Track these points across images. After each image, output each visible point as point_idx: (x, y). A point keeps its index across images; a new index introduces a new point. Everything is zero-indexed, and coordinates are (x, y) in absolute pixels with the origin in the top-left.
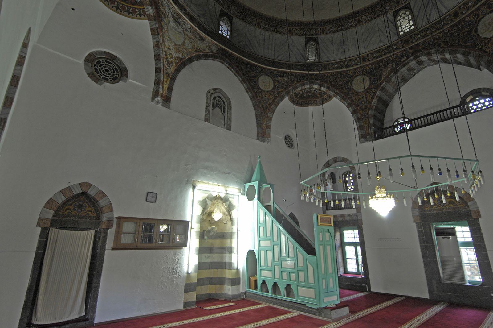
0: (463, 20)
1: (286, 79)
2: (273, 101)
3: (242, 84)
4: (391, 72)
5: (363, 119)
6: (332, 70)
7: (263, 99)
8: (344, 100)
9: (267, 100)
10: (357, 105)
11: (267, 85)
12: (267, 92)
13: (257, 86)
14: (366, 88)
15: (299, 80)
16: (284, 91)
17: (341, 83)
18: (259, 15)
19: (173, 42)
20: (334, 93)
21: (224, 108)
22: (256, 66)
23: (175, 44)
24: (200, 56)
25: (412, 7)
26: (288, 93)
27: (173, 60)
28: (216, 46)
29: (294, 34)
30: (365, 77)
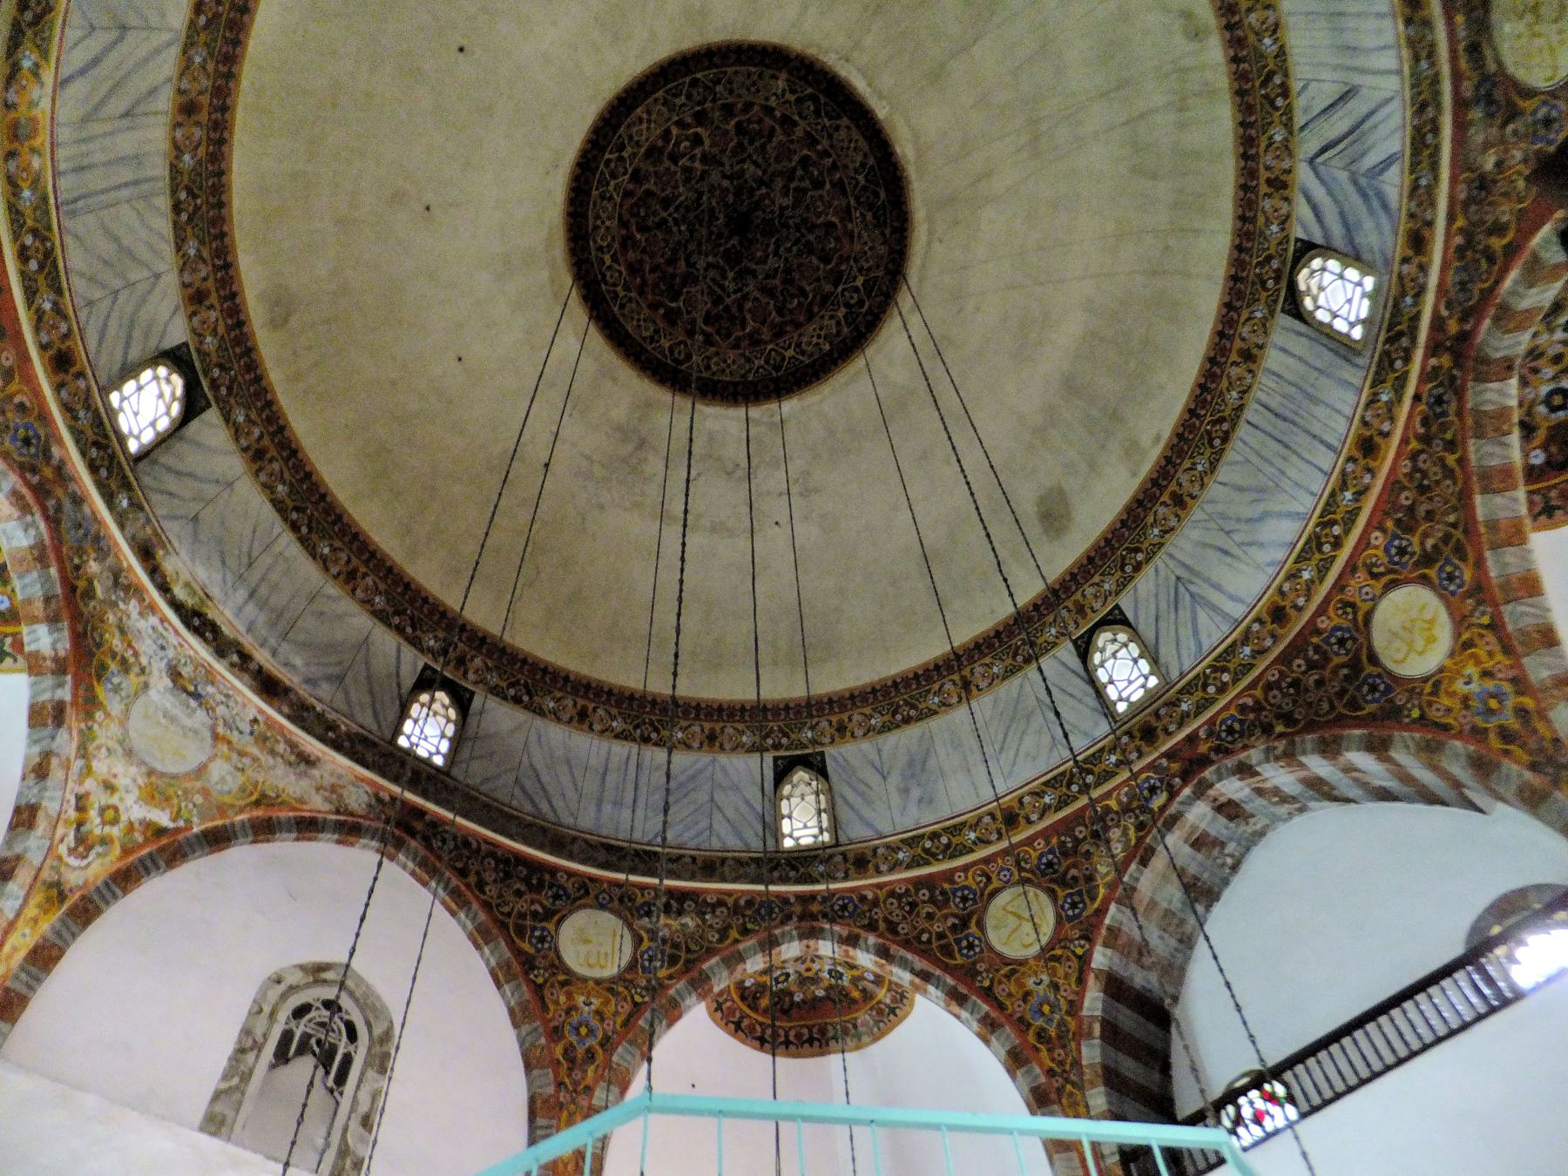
0: (1312, 628)
1: (690, 921)
2: (626, 1024)
3: (478, 947)
4: (1126, 863)
5: (1060, 1091)
6: (891, 870)
7: (575, 1018)
8: (961, 1005)
9: (594, 1022)
10: (1022, 1025)
11: (602, 951)
12: (598, 982)
13: (552, 954)
14: (1044, 940)
15: (749, 926)
16: (679, 979)
17: (937, 927)
18: (588, 686)
19: (143, 763)
20: (913, 971)
21: (348, 1060)
22: (554, 870)
23: (151, 772)
24: (269, 823)
25: (1130, 615)
26: (700, 984)
27: (115, 832)
28: (368, 789)
29: (727, 746)
30: (1031, 890)
